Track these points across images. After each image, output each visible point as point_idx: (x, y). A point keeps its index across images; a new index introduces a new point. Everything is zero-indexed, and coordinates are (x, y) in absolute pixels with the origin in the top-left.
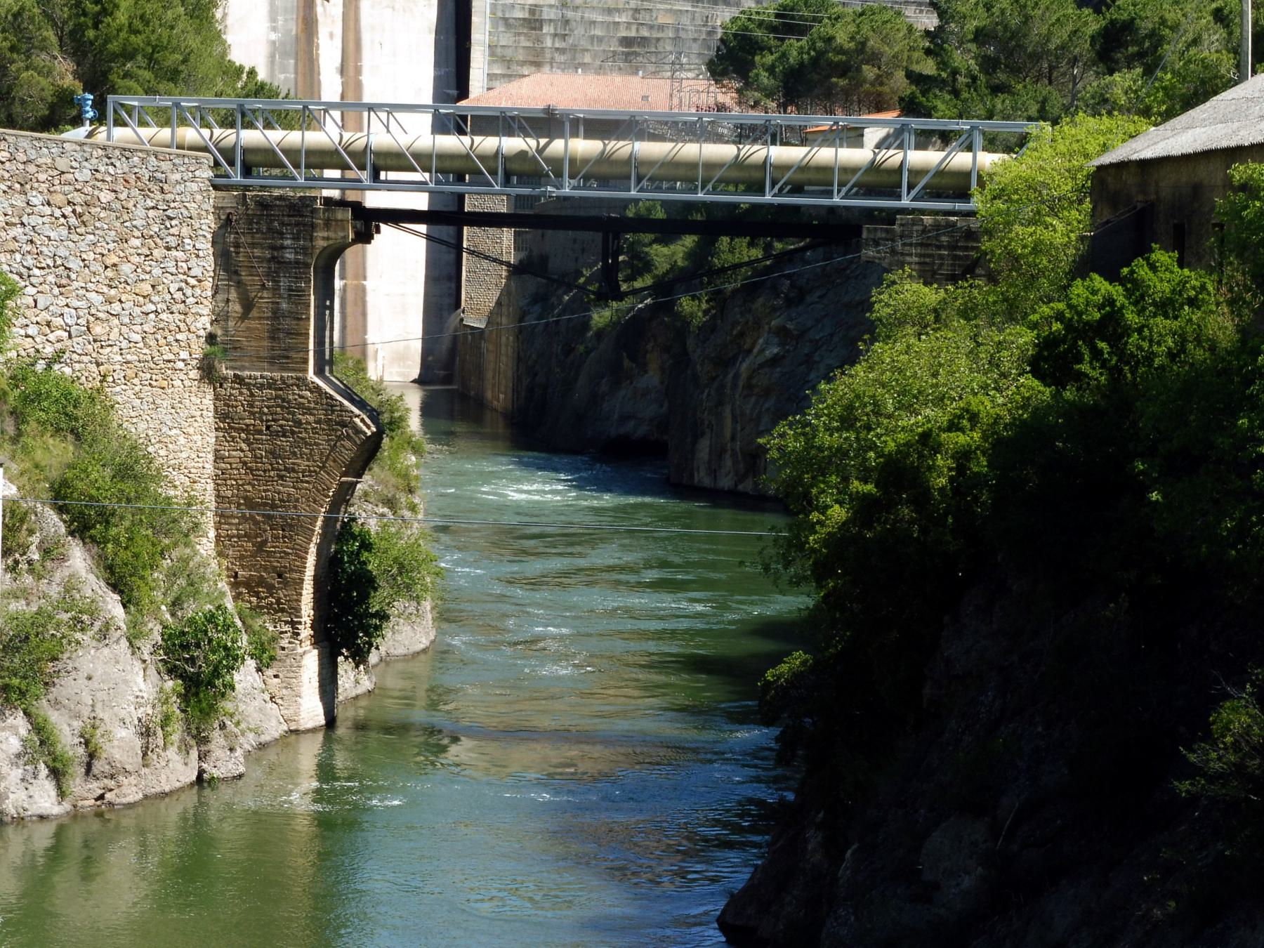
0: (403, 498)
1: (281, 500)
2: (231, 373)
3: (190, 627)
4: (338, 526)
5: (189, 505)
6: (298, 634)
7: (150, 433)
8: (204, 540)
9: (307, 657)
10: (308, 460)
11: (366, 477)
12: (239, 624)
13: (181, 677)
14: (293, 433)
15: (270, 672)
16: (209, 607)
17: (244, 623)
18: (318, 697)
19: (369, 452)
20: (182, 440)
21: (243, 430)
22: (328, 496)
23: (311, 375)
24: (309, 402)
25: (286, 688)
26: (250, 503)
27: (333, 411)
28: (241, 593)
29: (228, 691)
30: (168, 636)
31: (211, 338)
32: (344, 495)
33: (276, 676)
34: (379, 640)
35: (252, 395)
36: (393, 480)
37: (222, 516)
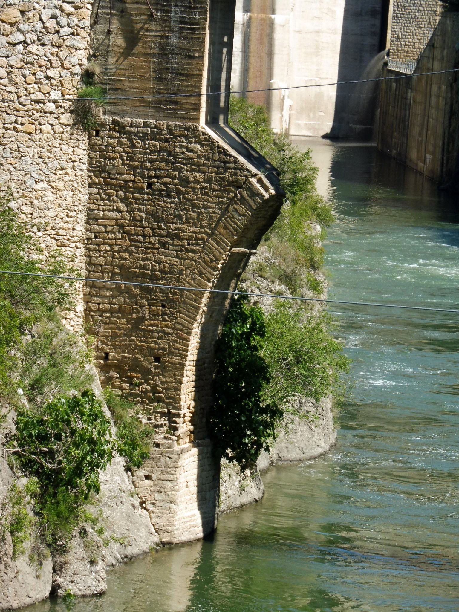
0: (304, 274)
1: (162, 271)
2: (109, 118)
3: (50, 414)
4: (227, 305)
5: (55, 272)
6: (176, 429)
7: (13, 185)
8: (72, 314)
9: (186, 455)
10: (195, 225)
11: (262, 248)
12: (108, 414)
13: (37, 473)
14: (179, 192)
15: (141, 472)
16: (73, 392)
17: (113, 412)
18: (195, 504)
19: (266, 217)
20: (49, 196)
21: (121, 187)
22: (215, 269)
23: (202, 125)
24: (199, 157)
25: (159, 492)
26: (126, 273)
27: (226, 169)
28: (111, 378)
29: (92, 492)
30: (24, 425)
31: (88, 77)
32: (235, 267)
33: (148, 478)
34: (270, 440)
35: (133, 146)
36: (293, 253)
37: (93, 286)
